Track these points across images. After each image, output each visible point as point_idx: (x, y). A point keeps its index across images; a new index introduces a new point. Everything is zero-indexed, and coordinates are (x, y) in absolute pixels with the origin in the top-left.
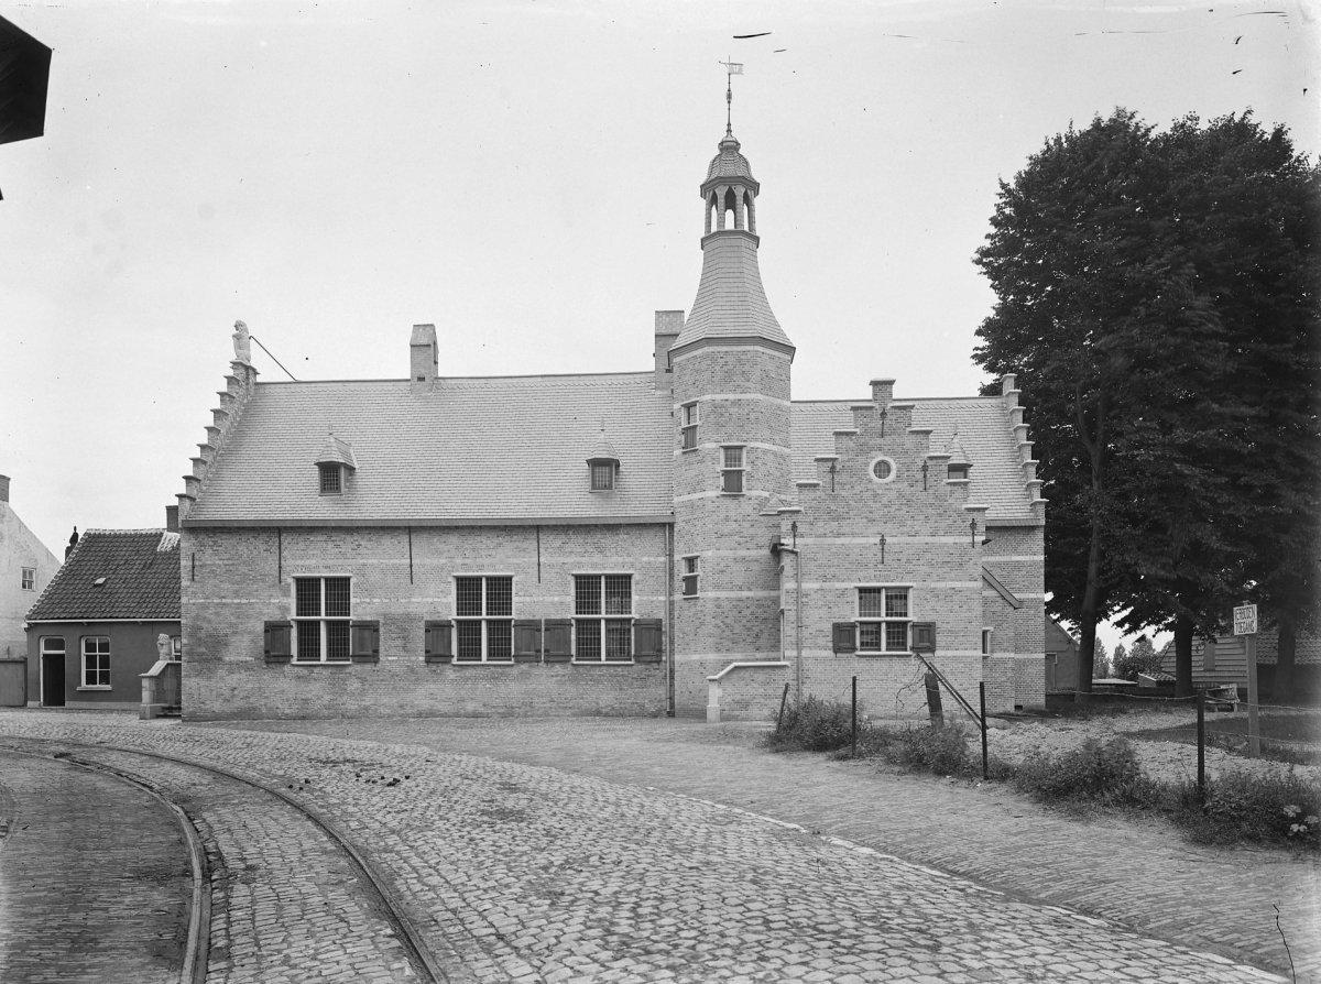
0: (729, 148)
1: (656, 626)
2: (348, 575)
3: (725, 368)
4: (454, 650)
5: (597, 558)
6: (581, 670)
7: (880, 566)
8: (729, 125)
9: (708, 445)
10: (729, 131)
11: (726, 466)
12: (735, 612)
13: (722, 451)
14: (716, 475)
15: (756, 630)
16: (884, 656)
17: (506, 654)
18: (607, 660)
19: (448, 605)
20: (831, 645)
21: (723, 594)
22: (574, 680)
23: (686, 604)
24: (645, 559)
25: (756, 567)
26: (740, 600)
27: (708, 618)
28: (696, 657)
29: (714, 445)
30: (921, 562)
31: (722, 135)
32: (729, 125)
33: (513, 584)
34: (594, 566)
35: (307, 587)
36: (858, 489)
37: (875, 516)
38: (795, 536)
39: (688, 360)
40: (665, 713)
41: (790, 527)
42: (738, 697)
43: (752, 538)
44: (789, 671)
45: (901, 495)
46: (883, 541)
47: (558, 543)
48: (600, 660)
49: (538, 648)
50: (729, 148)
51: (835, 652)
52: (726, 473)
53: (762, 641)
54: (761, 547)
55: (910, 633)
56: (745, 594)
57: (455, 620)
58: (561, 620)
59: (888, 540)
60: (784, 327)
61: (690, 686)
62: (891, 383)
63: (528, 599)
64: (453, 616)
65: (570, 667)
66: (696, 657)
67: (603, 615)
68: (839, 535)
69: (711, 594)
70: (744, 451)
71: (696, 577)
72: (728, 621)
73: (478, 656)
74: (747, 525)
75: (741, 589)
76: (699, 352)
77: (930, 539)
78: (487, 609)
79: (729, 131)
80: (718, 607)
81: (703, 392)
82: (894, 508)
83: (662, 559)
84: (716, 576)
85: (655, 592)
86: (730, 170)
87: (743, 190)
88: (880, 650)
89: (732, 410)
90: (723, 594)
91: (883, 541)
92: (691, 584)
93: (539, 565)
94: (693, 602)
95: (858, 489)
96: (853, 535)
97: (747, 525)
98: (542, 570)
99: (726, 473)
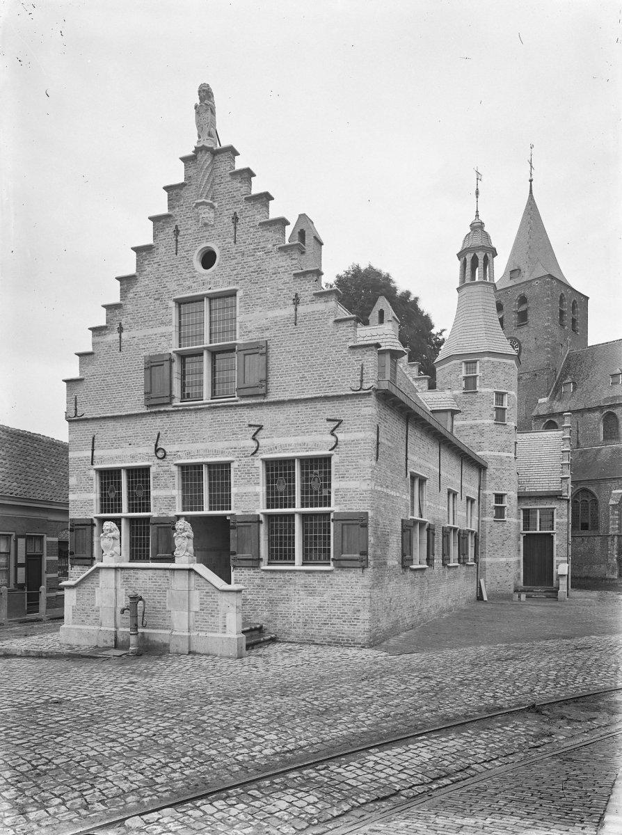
1: (361, 521)
2: (146, 463)
4: (264, 552)
8: (477, 212)
11: (467, 374)
13: (463, 364)
16: (300, 571)
17: (323, 556)
19: (90, 502)
23: (496, 524)
28: (503, 560)
32: (477, 212)
33: (232, 470)
57: (265, 514)
64: (261, 509)
66: (503, 560)
67: (298, 509)
70: (478, 364)
73: (288, 556)
78: (210, 502)
86: (477, 241)
94: (501, 523)
99: (466, 378)
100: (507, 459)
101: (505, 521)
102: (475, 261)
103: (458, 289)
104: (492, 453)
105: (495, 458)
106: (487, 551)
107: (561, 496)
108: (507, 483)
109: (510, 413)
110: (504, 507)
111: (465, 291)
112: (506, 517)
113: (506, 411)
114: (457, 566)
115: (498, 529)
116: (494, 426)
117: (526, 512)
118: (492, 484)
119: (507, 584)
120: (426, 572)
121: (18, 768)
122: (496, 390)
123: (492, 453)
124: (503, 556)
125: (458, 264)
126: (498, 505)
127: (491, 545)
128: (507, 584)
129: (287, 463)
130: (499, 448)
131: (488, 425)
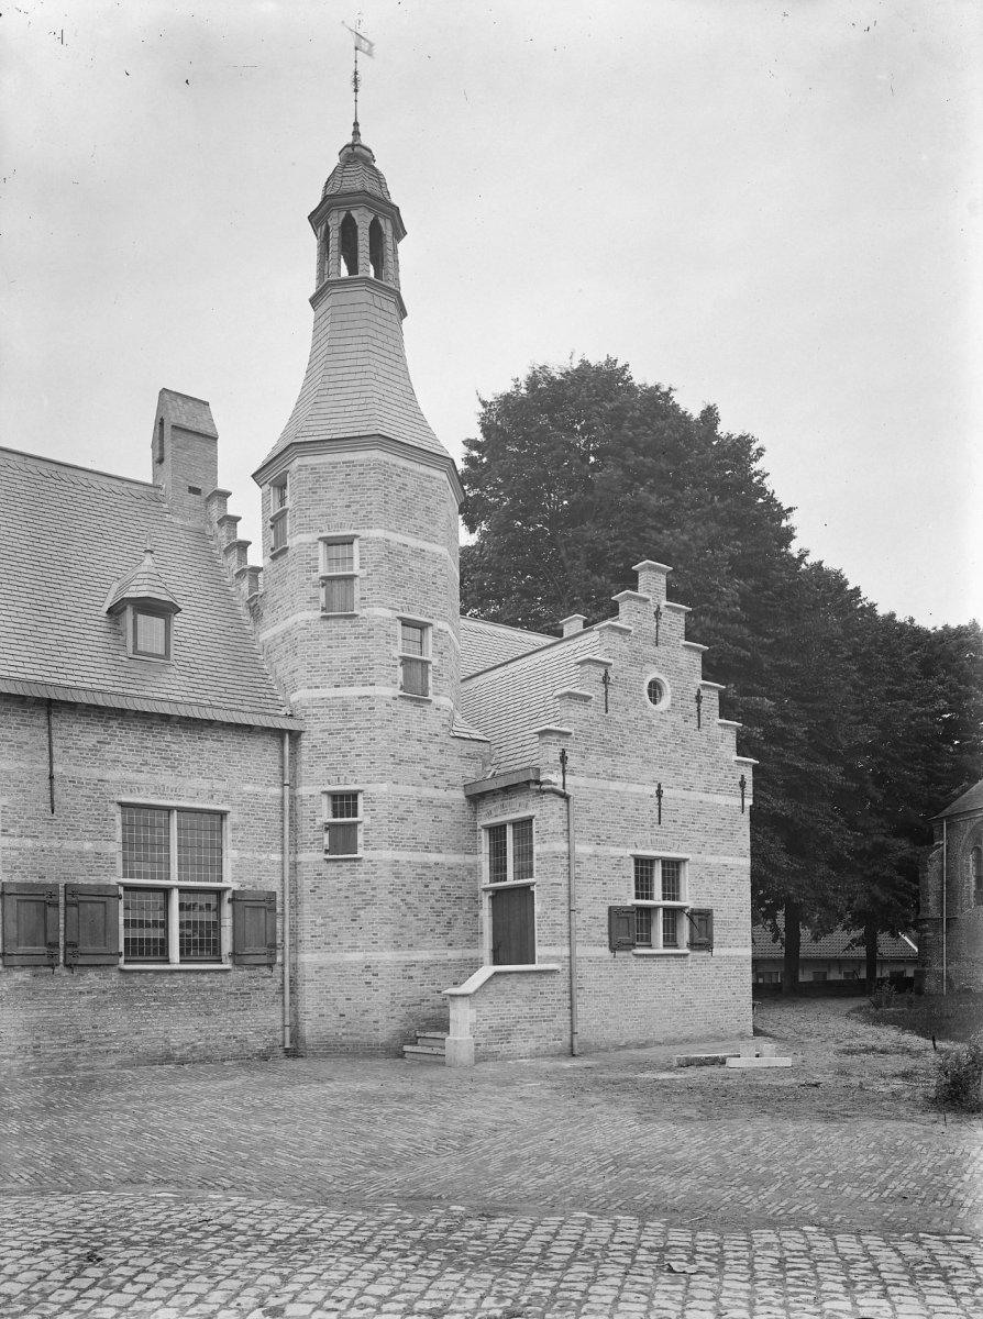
0: (356, 156)
1: (266, 903)
3: (403, 494)
5: (166, 778)
6: (137, 981)
7: (657, 827)
9: (378, 611)
10: (356, 133)
12: (420, 887)
14: (394, 663)
15: (448, 914)
16: (662, 955)
18: (182, 962)
20: (606, 938)
21: (404, 856)
22: (126, 998)
23: (333, 869)
24: (248, 788)
25: (446, 816)
26: (426, 866)
27: (382, 894)
29: (389, 614)
30: (696, 827)
31: (349, 139)
34: (160, 790)
35: (643, 865)
36: (633, 714)
37: (649, 755)
38: (564, 772)
39: (334, 465)
40: (280, 1051)
41: (558, 757)
42: (496, 1022)
43: (442, 769)
44: (559, 978)
45: (676, 732)
46: (659, 794)
47: (89, 740)
48: (167, 961)
49: (51, 939)
50: (356, 156)
51: (613, 949)
52: (406, 661)
53: (454, 934)
54: (452, 786)
55: (227, 910)
56: (433, 857)
58: (99, 887)
59: (666, 792)
60: (443, 442)
61: (342, 1004)
62: (239, 519)
63: (29, 843)
65: (115, 975)
68: (613, 777)
69: (388, 855)
71: (355, 824)
72: (410, 899)
74: (433, 748)
75: (427, 849)
76: (360, 456)
77: (704, 797)
79: (356, 133)
80: (397, 875)
81: (367, 522)
82: (671, 747)
83: (277, 791)
84: (394, 826)
85: (264, 847)
86: (355, 183)
87: (371, 217)
88: (167, 961)
89: (413, 564)
90: (404, 856)
91: (659, 794)
92: (342, 839)
93: (51, 778)
94: (346, 866)
95: (633, 714)
96: (630, 780)
97: (433, 748)
98: (58, 789)
100: (360, 704)
101: (360, 859)
102: (349, 227)
103: (314, 301)
104: (316, 693)
105: (326, 704)
106: (307, 937)
107: (538, 782)
108: (362, 763)
109: (367, 584)
110: (355, 824)
111: (326, 304)
112: (360, 850)
113: (357, 581)
114: (687, 955)
115: (339, 877)
116: (322, 627)
117: (497, 832)
118: (320, 770)
119: (370, 1018)
120: (689, 958)
121: (418, 1306)
122: (325, 534)
123: (316, 693)
124: (353, 948)
125: (310, 242)
126: (339, 820)
127: (319, 921)
128: (370, 1018)
129: (650, 861)
130: (336, 678)
131: (303, 625)
